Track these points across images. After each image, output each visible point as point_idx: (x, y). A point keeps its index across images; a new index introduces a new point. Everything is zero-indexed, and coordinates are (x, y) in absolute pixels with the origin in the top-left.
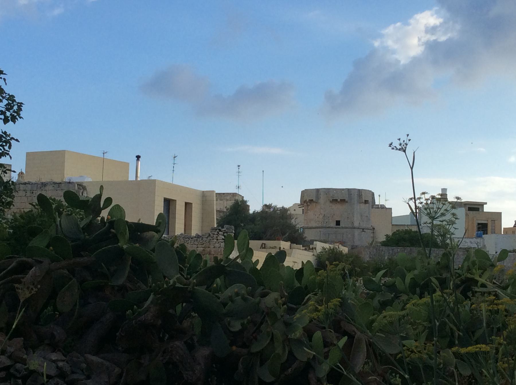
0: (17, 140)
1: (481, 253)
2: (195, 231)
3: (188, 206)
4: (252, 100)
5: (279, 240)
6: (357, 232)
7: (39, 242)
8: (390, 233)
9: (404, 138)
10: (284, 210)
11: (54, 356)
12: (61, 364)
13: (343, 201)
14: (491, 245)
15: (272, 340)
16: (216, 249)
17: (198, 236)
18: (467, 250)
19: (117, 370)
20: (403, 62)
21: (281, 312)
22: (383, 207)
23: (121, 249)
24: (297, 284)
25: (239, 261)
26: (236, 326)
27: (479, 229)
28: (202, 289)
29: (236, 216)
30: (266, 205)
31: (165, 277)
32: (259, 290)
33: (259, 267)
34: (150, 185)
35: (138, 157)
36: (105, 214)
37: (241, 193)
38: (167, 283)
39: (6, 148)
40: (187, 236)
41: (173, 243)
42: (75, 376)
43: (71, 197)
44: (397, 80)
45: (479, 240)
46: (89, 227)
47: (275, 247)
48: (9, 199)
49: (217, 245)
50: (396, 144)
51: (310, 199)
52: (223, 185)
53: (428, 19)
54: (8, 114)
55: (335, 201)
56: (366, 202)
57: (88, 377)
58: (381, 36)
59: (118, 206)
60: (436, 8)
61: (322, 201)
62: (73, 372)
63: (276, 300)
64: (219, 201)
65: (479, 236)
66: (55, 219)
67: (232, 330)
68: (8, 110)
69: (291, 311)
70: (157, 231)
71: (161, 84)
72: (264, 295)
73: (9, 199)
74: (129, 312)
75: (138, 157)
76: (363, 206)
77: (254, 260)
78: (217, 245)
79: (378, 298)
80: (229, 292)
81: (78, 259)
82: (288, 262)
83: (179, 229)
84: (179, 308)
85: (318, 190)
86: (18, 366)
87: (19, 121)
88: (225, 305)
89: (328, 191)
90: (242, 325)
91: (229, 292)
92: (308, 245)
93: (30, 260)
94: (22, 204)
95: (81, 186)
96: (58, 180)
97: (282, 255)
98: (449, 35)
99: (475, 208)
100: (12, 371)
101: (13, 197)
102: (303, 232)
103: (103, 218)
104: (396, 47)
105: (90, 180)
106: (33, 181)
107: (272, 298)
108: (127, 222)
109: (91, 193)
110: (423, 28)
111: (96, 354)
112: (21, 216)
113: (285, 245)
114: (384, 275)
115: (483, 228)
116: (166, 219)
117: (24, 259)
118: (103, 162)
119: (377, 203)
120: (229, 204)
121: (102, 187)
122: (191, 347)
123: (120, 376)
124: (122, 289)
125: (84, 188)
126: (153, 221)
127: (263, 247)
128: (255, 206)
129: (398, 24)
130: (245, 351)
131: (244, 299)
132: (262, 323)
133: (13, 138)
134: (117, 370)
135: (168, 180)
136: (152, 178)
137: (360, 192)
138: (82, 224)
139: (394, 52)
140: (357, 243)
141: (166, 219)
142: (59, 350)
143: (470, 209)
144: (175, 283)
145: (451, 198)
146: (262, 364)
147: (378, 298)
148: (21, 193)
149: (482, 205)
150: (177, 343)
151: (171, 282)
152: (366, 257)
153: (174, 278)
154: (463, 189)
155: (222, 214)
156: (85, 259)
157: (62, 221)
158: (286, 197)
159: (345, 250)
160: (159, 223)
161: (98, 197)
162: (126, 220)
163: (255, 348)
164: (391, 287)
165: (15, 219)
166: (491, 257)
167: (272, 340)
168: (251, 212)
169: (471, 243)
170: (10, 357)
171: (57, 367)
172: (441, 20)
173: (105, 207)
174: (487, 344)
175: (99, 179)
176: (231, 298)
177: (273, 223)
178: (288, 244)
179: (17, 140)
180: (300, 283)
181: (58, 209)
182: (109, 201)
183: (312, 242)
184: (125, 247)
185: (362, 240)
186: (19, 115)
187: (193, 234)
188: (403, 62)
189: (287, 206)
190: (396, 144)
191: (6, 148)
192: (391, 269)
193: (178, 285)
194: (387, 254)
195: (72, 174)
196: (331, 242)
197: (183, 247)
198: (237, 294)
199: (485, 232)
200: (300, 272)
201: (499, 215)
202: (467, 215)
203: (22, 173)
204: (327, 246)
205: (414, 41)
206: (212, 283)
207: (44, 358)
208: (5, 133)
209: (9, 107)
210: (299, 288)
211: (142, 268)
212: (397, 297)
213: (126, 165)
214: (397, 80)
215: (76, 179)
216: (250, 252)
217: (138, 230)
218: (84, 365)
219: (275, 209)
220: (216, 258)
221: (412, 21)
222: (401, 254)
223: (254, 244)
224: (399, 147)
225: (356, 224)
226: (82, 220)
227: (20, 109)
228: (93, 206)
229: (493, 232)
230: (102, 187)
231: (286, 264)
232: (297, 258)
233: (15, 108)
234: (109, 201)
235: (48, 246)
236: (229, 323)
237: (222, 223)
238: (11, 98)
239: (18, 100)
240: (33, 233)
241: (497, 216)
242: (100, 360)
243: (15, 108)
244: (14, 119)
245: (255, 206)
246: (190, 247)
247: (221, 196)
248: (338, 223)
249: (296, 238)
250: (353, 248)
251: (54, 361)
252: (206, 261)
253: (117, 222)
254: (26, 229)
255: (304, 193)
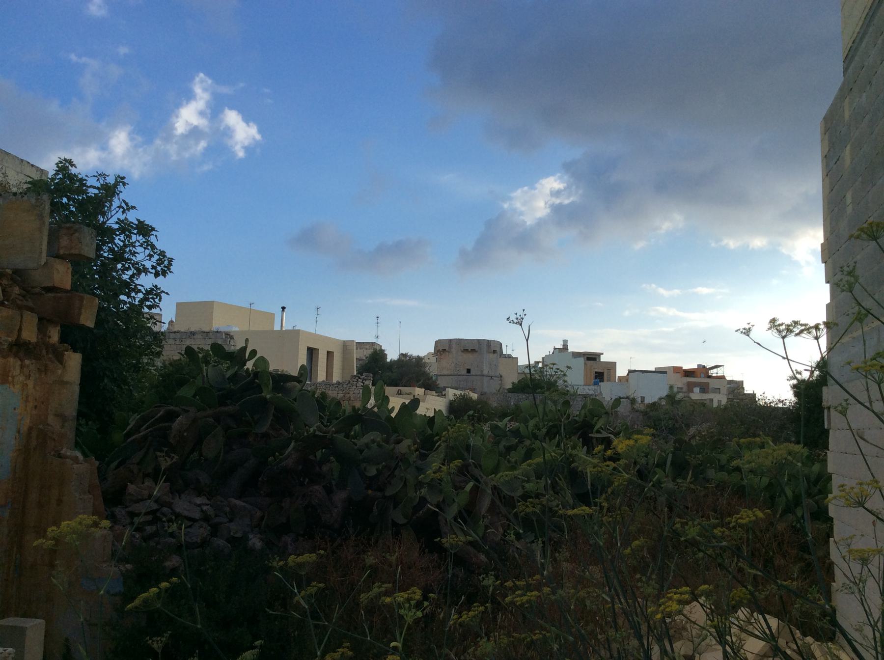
0: (167, 293)
1: (597, 403)
2: (336, 378)
3: (330, 354)
4: (392, 254)
5: (414, 386)
6: (486, 379)
7: (186, 392)
8: (516, 381)
9: (520, 312)
10: (419, 359)
11: (199, 500)
12: (205, 508)
13: (473, 351)
14: (607, 392)
15: (405, 484)
16: (353, 399)
17: (338, 383)
18: (585, 396)
19: (259, 513)
20: (528, 223)
21: (413, 458)
22: (510, 356)
23: (265, 399)
24: (430, 432)
25: (376, 409)
26: (372, 471)
27: (596, 377)
28: (341, 436)
29: (375, 365)
30: (402, 354)
31: (306, 425)
32: (394, 437)
33: (393, 415)
34: (295, 334)
35: (283, 308)
36: (250, 365)
37: (379, 342)
38: (308, 431)
39: (157, 300)
40: (328, 383)
41: (314, 393)
42: (217, 520)
43: (217, 348)
44: (525, 240)
45: (596, 387)
46: (234, 378)
47: (410, 394)
48: (158, 349)
49: (356, 392)
50: (513, 318)
51: (443, 348)
52: (364, 336)
53: (552, 183)
54: (159, 268)
55: (466, 351)
56: (495, 352)
57: (231, 521)
58: (510, 199)
59: (262, 358)
60: (559, 174)
61: (454, 350)
62: (216, 516)
63: (409, 446)
64: (359, 350)
65: (596, 384)
66: (202, 370)
67: (369, 475)
68: (159, 264)
69: (423, 457)
70: (299, 382)
71: (308, 239)
72: (398, 442)
73: (158, 349)
74: (271, 459)
75: (283, 308)
76: (491, 355)
77: (390, 407)
78: (356, 392)
79: (504, 443)
80: (366, 439)
81: (223, 409)
82: (421, 411)
83: (321, 376)
84: (319, 454)
85: (450, 340)
86: (165, 509)
87: (169, 276)
88: (361, 451)
89: (459, 341)
90: (377, 470)
91: (366, 439)
92: (440, 392)
93: (177, 409)
94: (172, 352)
95: (229, 336)
96: (207, 329)
97: (415, 403)
98: (571, 199)
99: (592, 358)
100: (158, 514)
101: (162, 347)
102: (437, 379)
103: (248, 369)
104: (523, 209)
105: (237, 329)
106: (182, 330)
107: (406, 445)
108: (271, 373)
109: (239, 344)
110: (548, 192)
111: (239, 498)
112: (171, 364)
113: (419, 391)
114: (510, 421)
115: (600, 376)
116: (307, 371)
117: (172, 408)
118: (250, 312)
119: (504, 353)
120: (369, 352)
121: (247, 340)
122: (329, 491)
123: (262, 518)
124: (266, 435)
125: (232, 337)
126: (295, 373)
127: (399, 393)
128: (392, 355)
129: (526, 188)
130: (379, 494)
131: (379, 446)
132: (395, 469)
133: (163, 292)
134: (259, 513)
135: (312, 330)
136: (297, 328)
137: (489, 342)
138: (229, 374)
139: (521, 214)
140: (486, 390)
141: (307, 371)
142: (204, 495)
143: (588, 359)
144: (315, 431)
145: (571, 349)
146: (395, 508)
147: (504, 443)
148: (171, 342)
149: (599, 355)
150: (317, 487)
151: (312, 430)
152: (494, 403)
153: (314, 427)
154: (581, 342)
155: (361, 362)
156: (230, 409)
157: (209, 371)
158: (421, 346)
159: (475, 396)
160: (300, 374)
161: (244, 349)
162: (271, 369)
163: (389, 492)
164: (516, 433)
165: (165, 367)
166: (605, 404)
167: (405, 484)
168: (388, 360)
169: (589, 390)
170: (156, 501)
171: (202, 511)
172: (565, 185)
173: (249, 359)
174: (590, 506)
175: (246, 328)
176: (367, 446)
177: (409, 371)
178: (423, 390)
179: (167, 293)
180: (432, 429)
181: (205, 357)
182: (254, 353)
183: (444, 389)
184: (268, 396)
185: (491, 387)
186: (169, 269)
187: (334, 381)
188: (528, 223)
189: (422, 355)
190: (513, 318)
191: (157, 300)
192: (516, 414)
193: (318, 433)
194: (513, 399)
195: (219, 323)
196: (462, 389)
197: (324, 395)
198: (373, 441)
199: (602, 380)
200: (431, 420)
201: (614, 364)
202: (585, 364)
203: (172, 321)
204: (458, 392)
205: (541, 204)
206: (350, 430)
207: (190, 502)
208: (156, 287)
209: (160, 262)
210: (429, 433)
211: (285, 416)
212: (521, 442)
213: (272, 316)
214: (525, 240)
215: (223, 328)
216: (386, 399)
217: (281, 380)
218: (227, 509)
219: (411, 357)
220: (354, 407)
221: (537, 185)
222: (525, 401)
223: (389, 390)
224: (515, 321)
225: (485, 372)
226: (227, 369)
227: (170, 264)
228: (238, 357)
229: (609, 380)
230: (247, 340)
231: (419, 412)
232: (431, 405)
233: (166, 263)
234: (254, 353)
235: (194, 396)
236: (365, 469)
237: (360, 372)
238: (162, 254)
239: (168, 255)
240: (181, 383)
241: (612, 366)
242: (243, 504)
243: (166, 263)
244: (164, 273)
245: (392, 355)
246: (332, 393)
247: (360, 345)
248: (469, 371)
249: (430, 385)
250: (482, 394)
251: (199, 505)
252: (344, 411)
253: (261, 373)
254: (175, 377)
255: (438, 343)
